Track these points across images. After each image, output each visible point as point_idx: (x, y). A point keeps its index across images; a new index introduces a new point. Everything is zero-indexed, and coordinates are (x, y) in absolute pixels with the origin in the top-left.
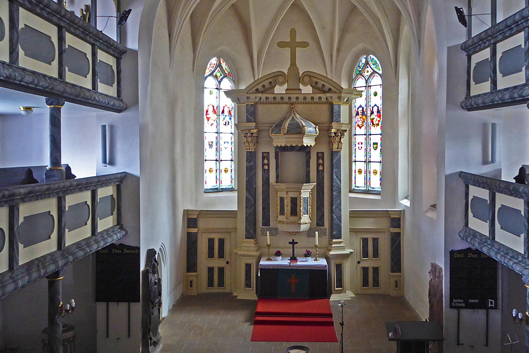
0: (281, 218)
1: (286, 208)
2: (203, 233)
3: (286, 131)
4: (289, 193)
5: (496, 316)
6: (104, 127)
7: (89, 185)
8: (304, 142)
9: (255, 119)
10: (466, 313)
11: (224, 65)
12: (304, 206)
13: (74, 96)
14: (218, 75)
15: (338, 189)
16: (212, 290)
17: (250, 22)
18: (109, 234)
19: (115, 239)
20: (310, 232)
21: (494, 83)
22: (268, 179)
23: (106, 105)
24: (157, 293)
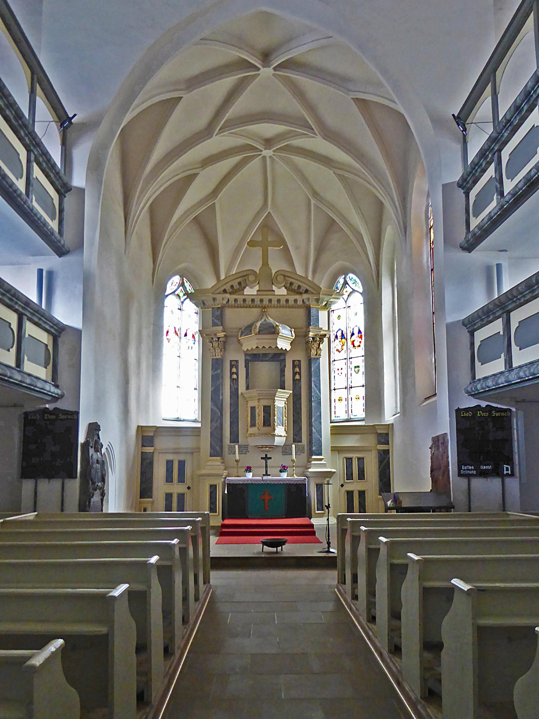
0: (251, 430)
1: (257, 418)
2: (160, 454)
4: (261, 401)
5: (513, 485)
6: (40, 271)
10: (478, 483)
11: (187, 285)
14: (181, 294)
15: (318, 400)
17: (217, 241)
22: (237, 389)
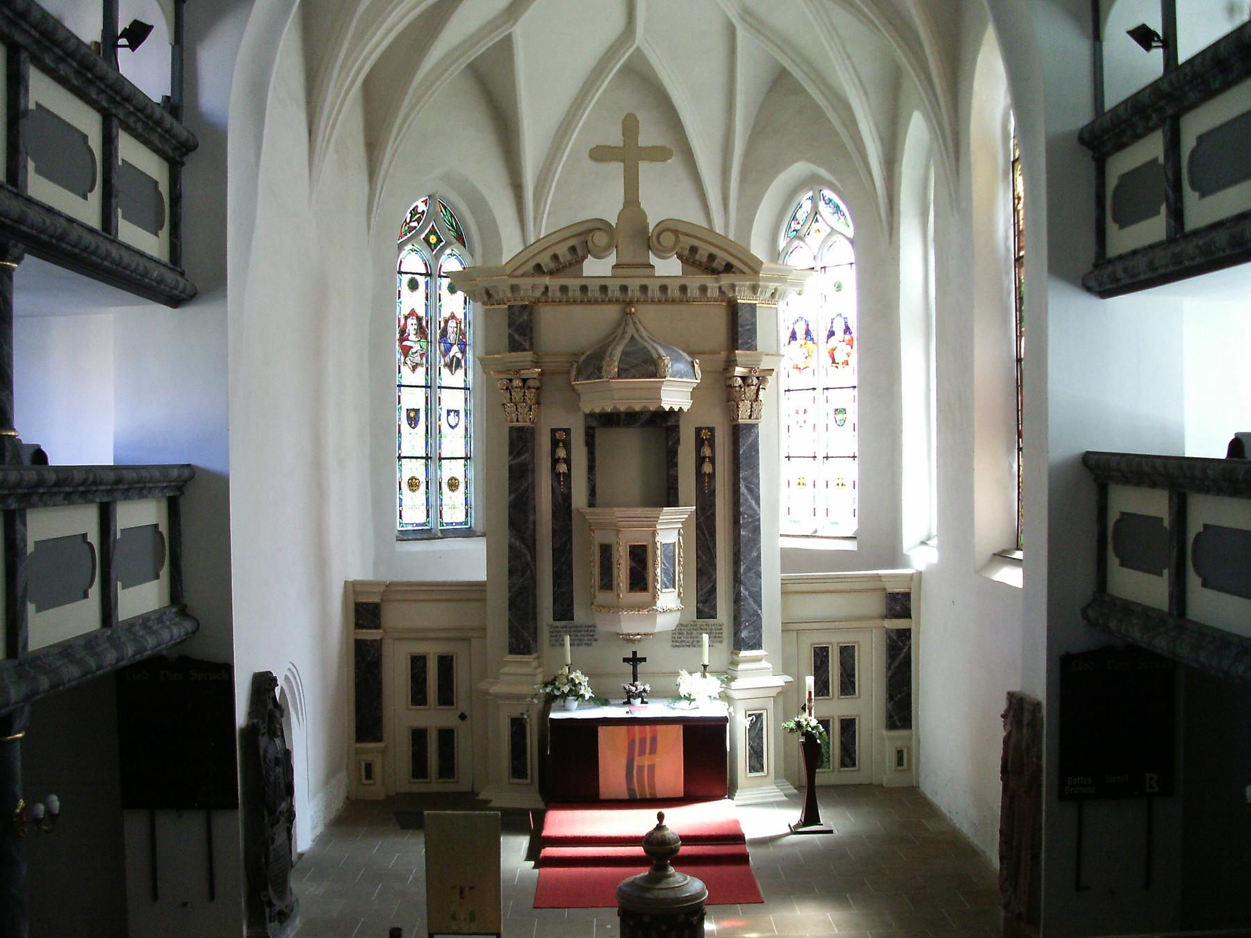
3: (616, 369)
7: (94, 488)
8: (663, 399)
9: (532, 344)
12: (665, 565)
13: (51, 237)
16: (420, 787)
18: (151, 627)
19: (166, 641)
20: (680, 634)
21: (1177, 215)
22: (567, 497)
23: (138, 277)
24: (282, 786)
